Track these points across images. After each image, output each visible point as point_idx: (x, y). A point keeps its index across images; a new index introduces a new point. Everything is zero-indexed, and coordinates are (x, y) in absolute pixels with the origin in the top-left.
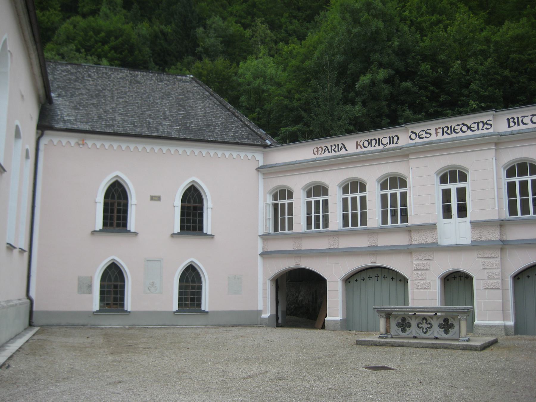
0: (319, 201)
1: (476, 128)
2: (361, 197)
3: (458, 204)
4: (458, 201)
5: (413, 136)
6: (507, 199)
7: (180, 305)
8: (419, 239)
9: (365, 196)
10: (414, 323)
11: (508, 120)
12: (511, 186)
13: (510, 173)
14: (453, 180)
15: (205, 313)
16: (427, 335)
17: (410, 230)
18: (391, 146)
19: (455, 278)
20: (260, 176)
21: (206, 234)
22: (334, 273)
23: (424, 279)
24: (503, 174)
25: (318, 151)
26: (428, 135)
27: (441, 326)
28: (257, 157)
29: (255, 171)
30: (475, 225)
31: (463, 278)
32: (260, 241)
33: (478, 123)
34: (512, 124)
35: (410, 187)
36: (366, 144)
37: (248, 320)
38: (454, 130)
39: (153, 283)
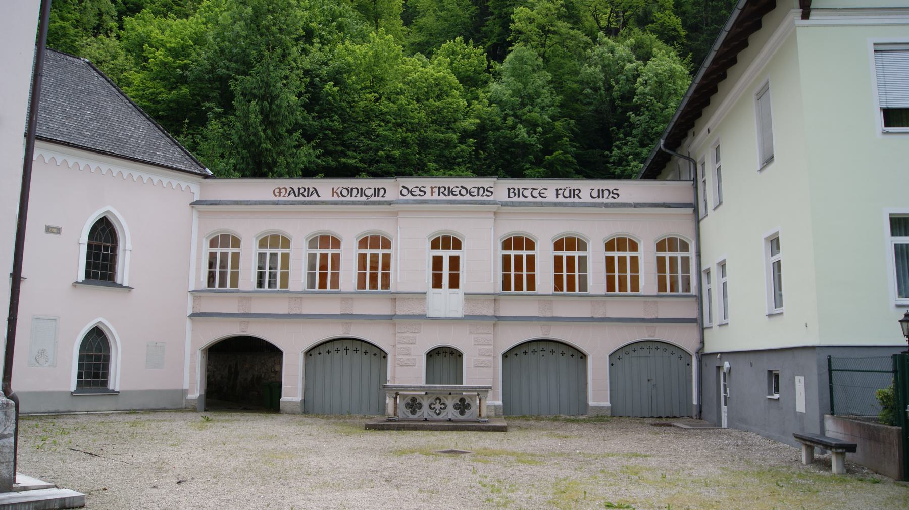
0: (315, 255)
1: (476, 193)
2: (333, 255)
3: (434, 274)
4: (433, 270)
5: (405, 192)
6: (460, 272)
7: (79, 383)
8: (403, 309)
9: (533, 256)
10: (425, 403)
11: (509, 190)
12: (506, 259)
13: (506, 245)
14: (446, 247)
15: (114, 393)
16: (440, 417)
17: (395, 298)
18: (376, 199)
19: (438, 354)
20: (195, 215)
21: (121, 286)
22: (293, 345)
23: (409, 354)
24: (500, 246)
25: (280, 192)
26: (422, 194)
27: (456, 407)
28: (194, 188)
29: (189, 208)
30: (470, 297)
31: (448, 355)
32: (190, 299)
33: (479, 189)
34: (512, 195)
35: (397, 249)
36: (345, 193)
37: (170, 405)
38: (452, 192)
39: (44, 351)
